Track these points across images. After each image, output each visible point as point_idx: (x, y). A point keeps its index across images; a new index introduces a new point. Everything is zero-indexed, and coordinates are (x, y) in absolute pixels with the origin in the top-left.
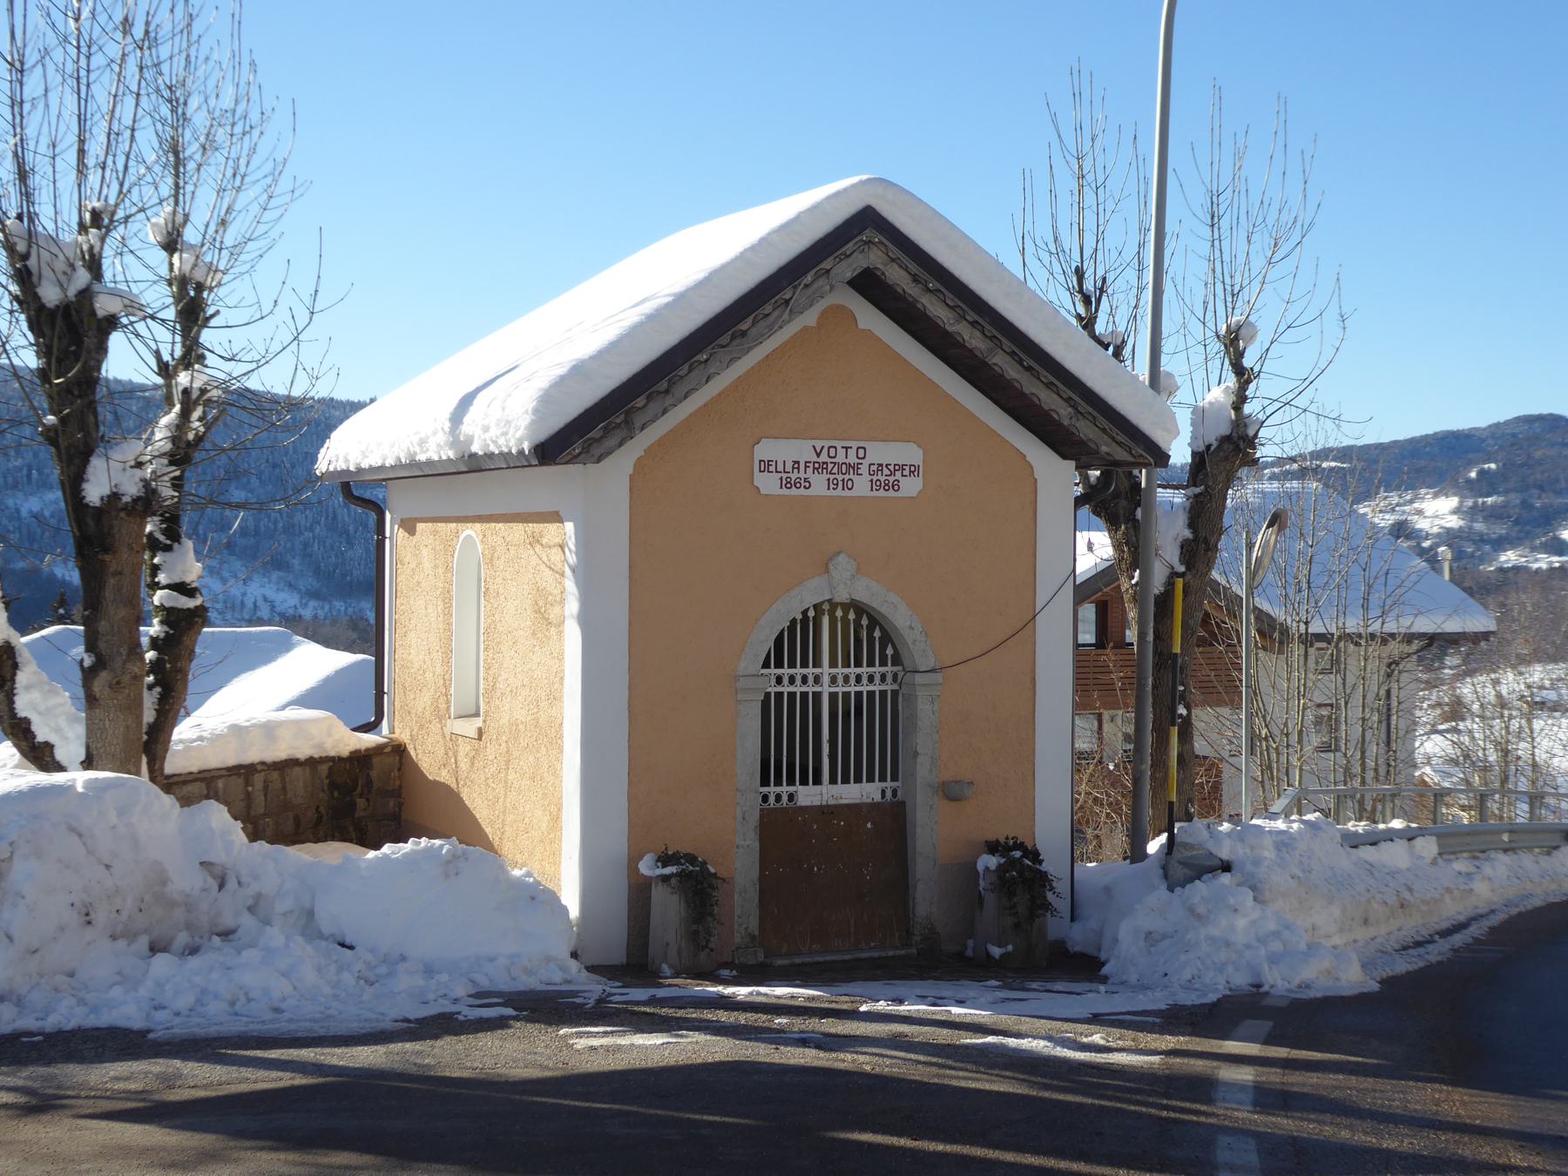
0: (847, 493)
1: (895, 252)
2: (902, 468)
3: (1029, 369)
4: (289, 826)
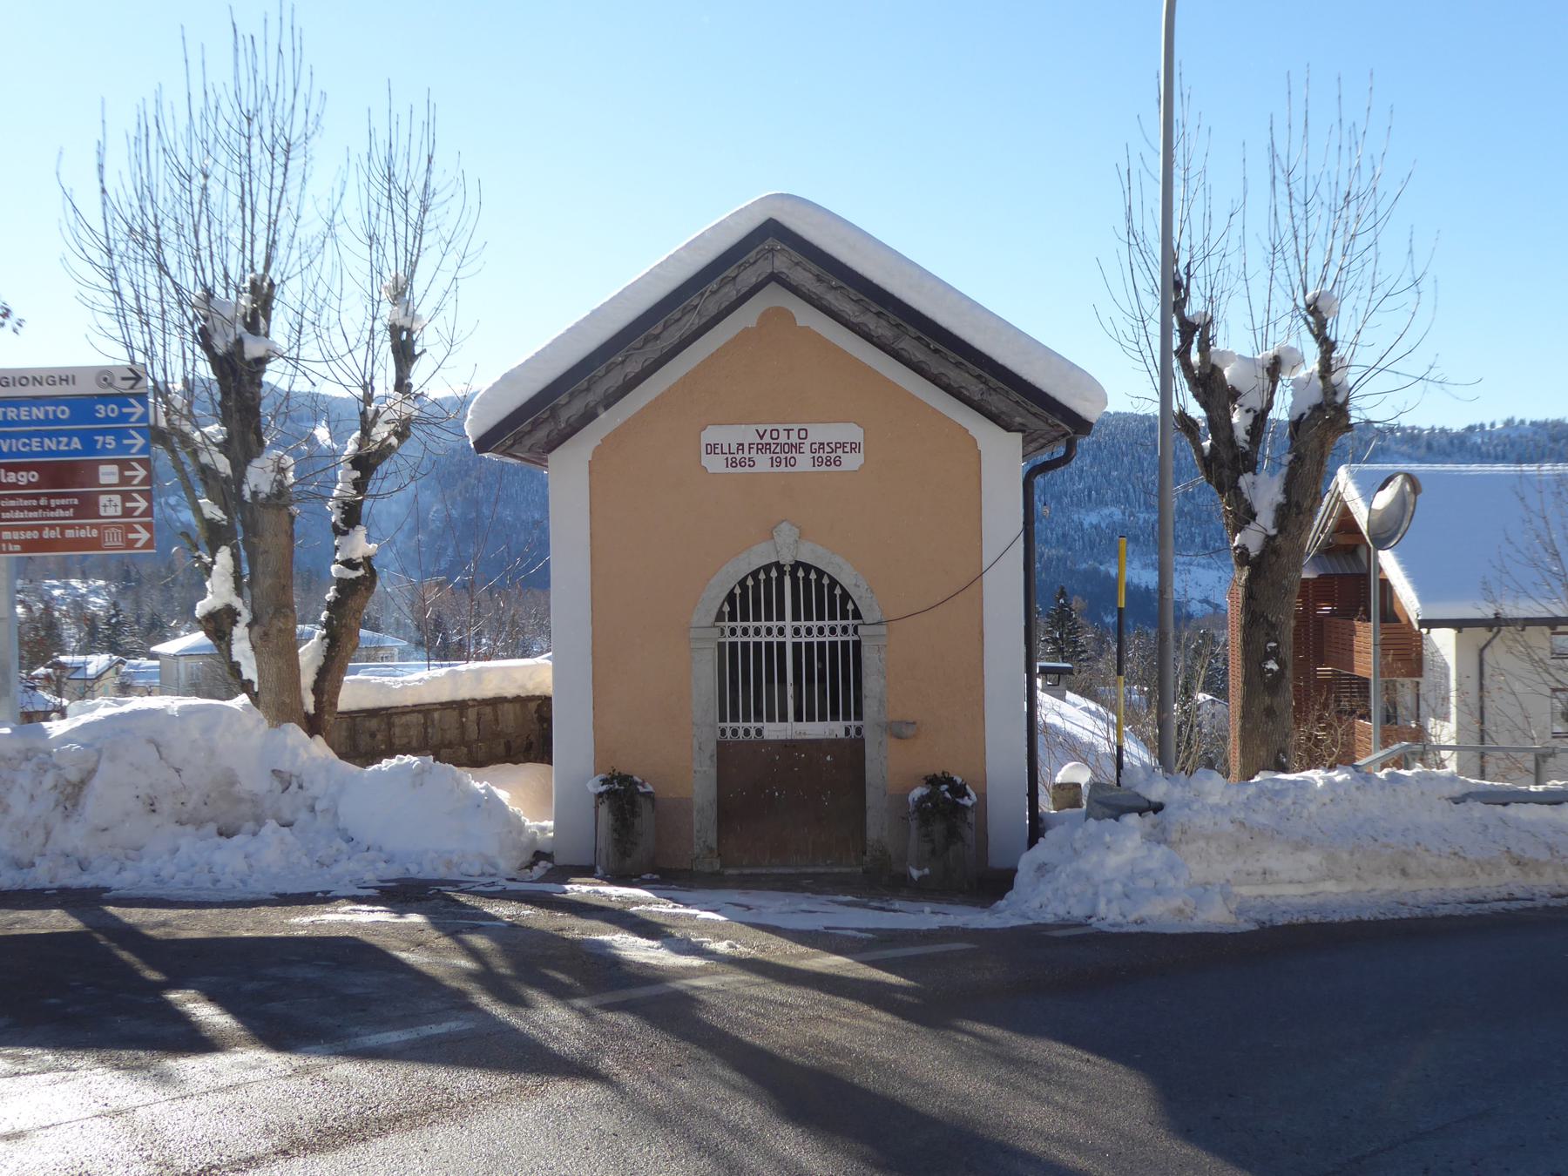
0: (790, 469)
1: (797, 257)
2: (843, 445)
3: (936, 351)
4: (501, 749)
